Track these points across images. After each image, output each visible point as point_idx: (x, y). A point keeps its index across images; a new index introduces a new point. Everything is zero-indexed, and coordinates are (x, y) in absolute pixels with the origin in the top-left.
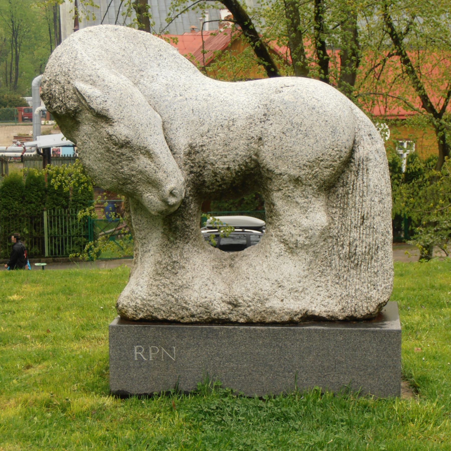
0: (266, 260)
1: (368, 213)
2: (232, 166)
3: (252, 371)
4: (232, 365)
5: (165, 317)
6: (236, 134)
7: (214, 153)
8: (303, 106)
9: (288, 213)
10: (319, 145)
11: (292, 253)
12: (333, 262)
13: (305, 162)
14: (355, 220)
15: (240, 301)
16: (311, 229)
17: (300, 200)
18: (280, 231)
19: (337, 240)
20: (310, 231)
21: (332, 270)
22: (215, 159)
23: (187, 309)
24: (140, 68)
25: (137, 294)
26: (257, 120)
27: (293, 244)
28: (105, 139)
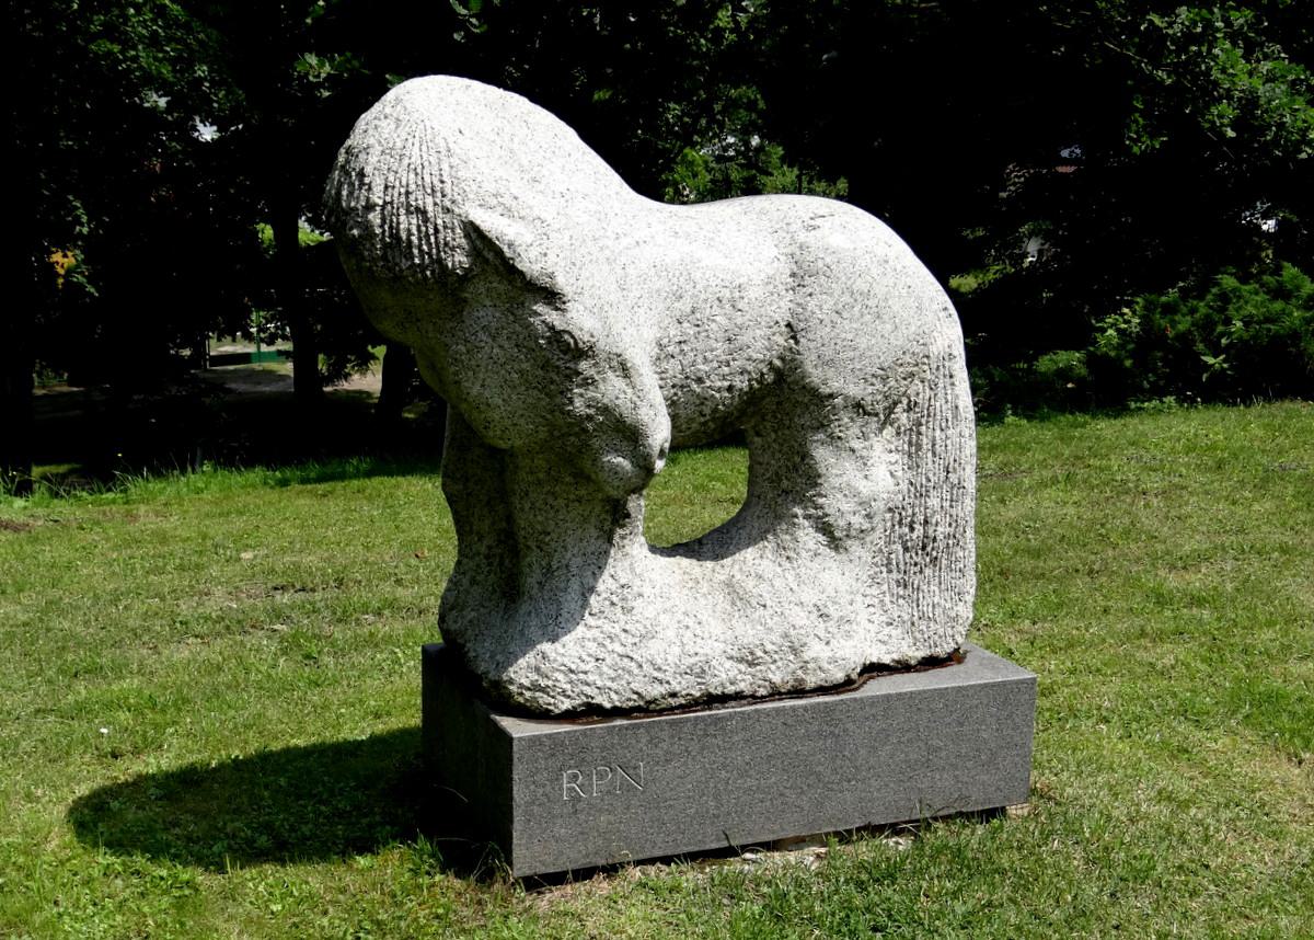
0: (788, 565)
1: (955, 461)
2: (738, 384)
3: (785, 788)
4: (750, 782)
5: (618, 704)
6: (748, 317)
7: (705, 358)
8: (867, 256)
9: (834, 471)
10: (900, 334)
11: (836, 549)
12: (893, 556)
13: (874, 369)
14: (935, 474)
15: (759, 654)
16: (875, 500)
17: (856, 444)
18: (816, 509)
19: (900, 514)
20: (873, 504)
21: (890, 571)
22: (707, 369)
23: (661, 682)
24: (533, 174)
25: (555, 660)
26: (781, 287)
27: (842, 531)
28: (541, 341)
